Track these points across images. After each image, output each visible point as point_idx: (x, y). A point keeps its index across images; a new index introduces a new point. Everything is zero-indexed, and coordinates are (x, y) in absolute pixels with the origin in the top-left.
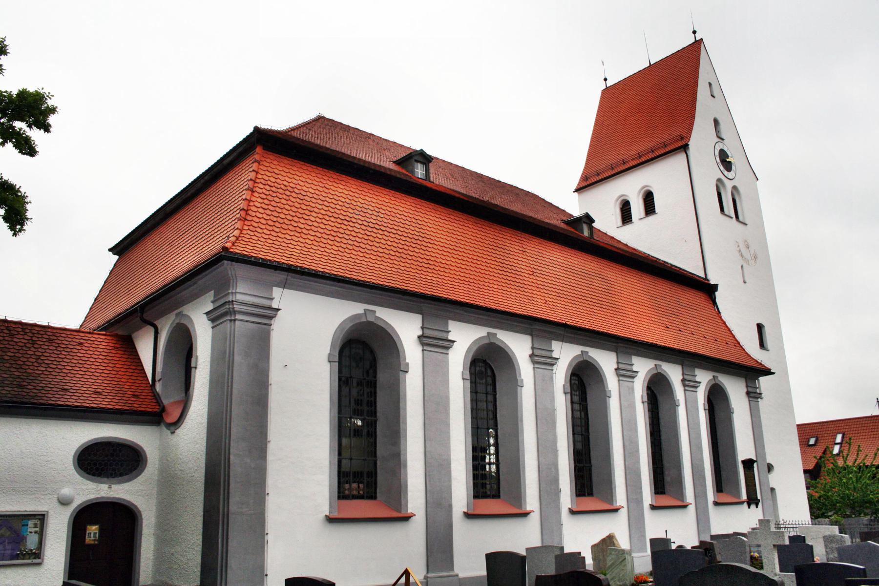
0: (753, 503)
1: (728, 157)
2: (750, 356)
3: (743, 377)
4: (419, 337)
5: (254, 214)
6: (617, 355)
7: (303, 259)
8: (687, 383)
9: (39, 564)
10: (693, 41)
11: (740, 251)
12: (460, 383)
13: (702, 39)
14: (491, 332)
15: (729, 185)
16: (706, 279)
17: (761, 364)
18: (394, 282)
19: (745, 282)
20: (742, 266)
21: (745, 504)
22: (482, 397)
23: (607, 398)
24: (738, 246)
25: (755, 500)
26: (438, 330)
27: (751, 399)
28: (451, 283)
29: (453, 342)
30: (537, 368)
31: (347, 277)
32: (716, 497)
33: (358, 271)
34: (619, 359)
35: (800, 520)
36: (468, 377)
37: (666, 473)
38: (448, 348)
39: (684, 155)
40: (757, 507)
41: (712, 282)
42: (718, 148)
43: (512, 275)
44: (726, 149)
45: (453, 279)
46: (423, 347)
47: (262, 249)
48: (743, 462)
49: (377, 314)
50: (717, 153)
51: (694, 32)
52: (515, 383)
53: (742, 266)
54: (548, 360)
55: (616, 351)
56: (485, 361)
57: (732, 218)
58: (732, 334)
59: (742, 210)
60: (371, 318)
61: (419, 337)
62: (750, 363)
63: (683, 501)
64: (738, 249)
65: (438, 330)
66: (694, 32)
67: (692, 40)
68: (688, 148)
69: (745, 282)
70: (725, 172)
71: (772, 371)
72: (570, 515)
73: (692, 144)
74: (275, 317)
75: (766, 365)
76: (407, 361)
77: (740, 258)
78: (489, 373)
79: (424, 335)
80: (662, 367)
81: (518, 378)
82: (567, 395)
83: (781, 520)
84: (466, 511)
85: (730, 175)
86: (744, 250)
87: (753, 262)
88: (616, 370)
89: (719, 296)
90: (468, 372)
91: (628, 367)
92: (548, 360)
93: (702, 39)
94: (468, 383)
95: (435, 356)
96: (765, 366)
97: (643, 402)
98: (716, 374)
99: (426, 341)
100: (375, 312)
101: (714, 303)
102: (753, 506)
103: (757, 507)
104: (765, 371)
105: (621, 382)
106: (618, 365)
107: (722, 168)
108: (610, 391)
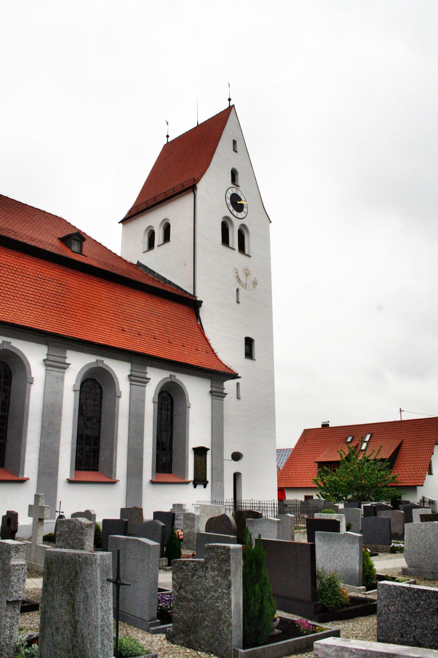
0: (200, 484)
1: (240, 200)
2: (222, 362)
3: (209, 379)
4: (44, 360)
5: (204, 350)
6: (132, 365)
7: (44, 325)
8: (133, 378)
9: (422, 486)
10: (228, 106)
11: (238, 276)
12: (152, 405)
13: (233, 106)
14: (4, 340)
15: (237, 224)
16: (194, 296)
17: (230, 369)
18: (124, 346)
19: (238, 302)
20: (238, 290)
21: (191, 485)
22: (90, 402)
23: (28, 384)
24: (237, 273)
25: (203, 481)
26: (52, 355)
27: (213, 397)
28: (149, 343)
29: (149, 379)
30: (49, 370)
31: (65, 335)
32: (155, 477)
33: (69, 331)
34: (133, 368)
35: (266, 501)
36: (157, 401)
37: (101, 454)
38: (146, 383)
39: (192, 195)
40: (205, 487)
41: (198, 299)
42: (231, 192)
43: (111, 320)
44: (239, 194)
45: (144, 339)
46: (131, 382)
47: (66, 330)
48: (194, 449)
49: (12, 344)
50: (229, 196)
51: (230, 100)
52: (116, 396)
53: (238, 290)
54: (145, 380)
55: (47, 344)
56: (94, 380)
57: (234, 249)
58: (208, 343)
59: (249, 244)
60: (100, 365)
61: (44, 360)
62: (222, 369)
63: (111, 478)
64: (237, 275)
65: (52, 355)
66: (230, 100)
67: (226, 106)
68: (196, 188)
69: (238, 302)
70: (235, 213)
71: (239, 375)
72: (150, 484)
73: (199, 186)
74: (148, 383)
75: (234, 370)
76: (120, 390)
77: (237, 282)
78: (169, 398)
79: (48, 359)
80: (105, 362)
81: (28, 377)
82: (76, 392)
83: (243, 500)
84: (69, 478)
85: (240, 215)
86: (242, 278)
87: (251, 287)
88: (129, 376)
89: (203, 313)
90: (157, 397)
91: (61, 360)
92: (145, 380)
93: (233, 106)
94: (156, 405)
95: (56, 373)
96: (232, 371)
97: (154, 402)
98: (173, 373)
99: (133, 378)
100: (103, 361)
101: (198, 317)
102: (200, 487)
103: (205, 487)
104: (232, 376)
105: (132, 386)
106: (48, 357)
107: (231, 208)
108: (33, 378)
